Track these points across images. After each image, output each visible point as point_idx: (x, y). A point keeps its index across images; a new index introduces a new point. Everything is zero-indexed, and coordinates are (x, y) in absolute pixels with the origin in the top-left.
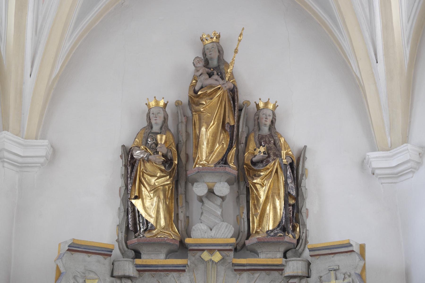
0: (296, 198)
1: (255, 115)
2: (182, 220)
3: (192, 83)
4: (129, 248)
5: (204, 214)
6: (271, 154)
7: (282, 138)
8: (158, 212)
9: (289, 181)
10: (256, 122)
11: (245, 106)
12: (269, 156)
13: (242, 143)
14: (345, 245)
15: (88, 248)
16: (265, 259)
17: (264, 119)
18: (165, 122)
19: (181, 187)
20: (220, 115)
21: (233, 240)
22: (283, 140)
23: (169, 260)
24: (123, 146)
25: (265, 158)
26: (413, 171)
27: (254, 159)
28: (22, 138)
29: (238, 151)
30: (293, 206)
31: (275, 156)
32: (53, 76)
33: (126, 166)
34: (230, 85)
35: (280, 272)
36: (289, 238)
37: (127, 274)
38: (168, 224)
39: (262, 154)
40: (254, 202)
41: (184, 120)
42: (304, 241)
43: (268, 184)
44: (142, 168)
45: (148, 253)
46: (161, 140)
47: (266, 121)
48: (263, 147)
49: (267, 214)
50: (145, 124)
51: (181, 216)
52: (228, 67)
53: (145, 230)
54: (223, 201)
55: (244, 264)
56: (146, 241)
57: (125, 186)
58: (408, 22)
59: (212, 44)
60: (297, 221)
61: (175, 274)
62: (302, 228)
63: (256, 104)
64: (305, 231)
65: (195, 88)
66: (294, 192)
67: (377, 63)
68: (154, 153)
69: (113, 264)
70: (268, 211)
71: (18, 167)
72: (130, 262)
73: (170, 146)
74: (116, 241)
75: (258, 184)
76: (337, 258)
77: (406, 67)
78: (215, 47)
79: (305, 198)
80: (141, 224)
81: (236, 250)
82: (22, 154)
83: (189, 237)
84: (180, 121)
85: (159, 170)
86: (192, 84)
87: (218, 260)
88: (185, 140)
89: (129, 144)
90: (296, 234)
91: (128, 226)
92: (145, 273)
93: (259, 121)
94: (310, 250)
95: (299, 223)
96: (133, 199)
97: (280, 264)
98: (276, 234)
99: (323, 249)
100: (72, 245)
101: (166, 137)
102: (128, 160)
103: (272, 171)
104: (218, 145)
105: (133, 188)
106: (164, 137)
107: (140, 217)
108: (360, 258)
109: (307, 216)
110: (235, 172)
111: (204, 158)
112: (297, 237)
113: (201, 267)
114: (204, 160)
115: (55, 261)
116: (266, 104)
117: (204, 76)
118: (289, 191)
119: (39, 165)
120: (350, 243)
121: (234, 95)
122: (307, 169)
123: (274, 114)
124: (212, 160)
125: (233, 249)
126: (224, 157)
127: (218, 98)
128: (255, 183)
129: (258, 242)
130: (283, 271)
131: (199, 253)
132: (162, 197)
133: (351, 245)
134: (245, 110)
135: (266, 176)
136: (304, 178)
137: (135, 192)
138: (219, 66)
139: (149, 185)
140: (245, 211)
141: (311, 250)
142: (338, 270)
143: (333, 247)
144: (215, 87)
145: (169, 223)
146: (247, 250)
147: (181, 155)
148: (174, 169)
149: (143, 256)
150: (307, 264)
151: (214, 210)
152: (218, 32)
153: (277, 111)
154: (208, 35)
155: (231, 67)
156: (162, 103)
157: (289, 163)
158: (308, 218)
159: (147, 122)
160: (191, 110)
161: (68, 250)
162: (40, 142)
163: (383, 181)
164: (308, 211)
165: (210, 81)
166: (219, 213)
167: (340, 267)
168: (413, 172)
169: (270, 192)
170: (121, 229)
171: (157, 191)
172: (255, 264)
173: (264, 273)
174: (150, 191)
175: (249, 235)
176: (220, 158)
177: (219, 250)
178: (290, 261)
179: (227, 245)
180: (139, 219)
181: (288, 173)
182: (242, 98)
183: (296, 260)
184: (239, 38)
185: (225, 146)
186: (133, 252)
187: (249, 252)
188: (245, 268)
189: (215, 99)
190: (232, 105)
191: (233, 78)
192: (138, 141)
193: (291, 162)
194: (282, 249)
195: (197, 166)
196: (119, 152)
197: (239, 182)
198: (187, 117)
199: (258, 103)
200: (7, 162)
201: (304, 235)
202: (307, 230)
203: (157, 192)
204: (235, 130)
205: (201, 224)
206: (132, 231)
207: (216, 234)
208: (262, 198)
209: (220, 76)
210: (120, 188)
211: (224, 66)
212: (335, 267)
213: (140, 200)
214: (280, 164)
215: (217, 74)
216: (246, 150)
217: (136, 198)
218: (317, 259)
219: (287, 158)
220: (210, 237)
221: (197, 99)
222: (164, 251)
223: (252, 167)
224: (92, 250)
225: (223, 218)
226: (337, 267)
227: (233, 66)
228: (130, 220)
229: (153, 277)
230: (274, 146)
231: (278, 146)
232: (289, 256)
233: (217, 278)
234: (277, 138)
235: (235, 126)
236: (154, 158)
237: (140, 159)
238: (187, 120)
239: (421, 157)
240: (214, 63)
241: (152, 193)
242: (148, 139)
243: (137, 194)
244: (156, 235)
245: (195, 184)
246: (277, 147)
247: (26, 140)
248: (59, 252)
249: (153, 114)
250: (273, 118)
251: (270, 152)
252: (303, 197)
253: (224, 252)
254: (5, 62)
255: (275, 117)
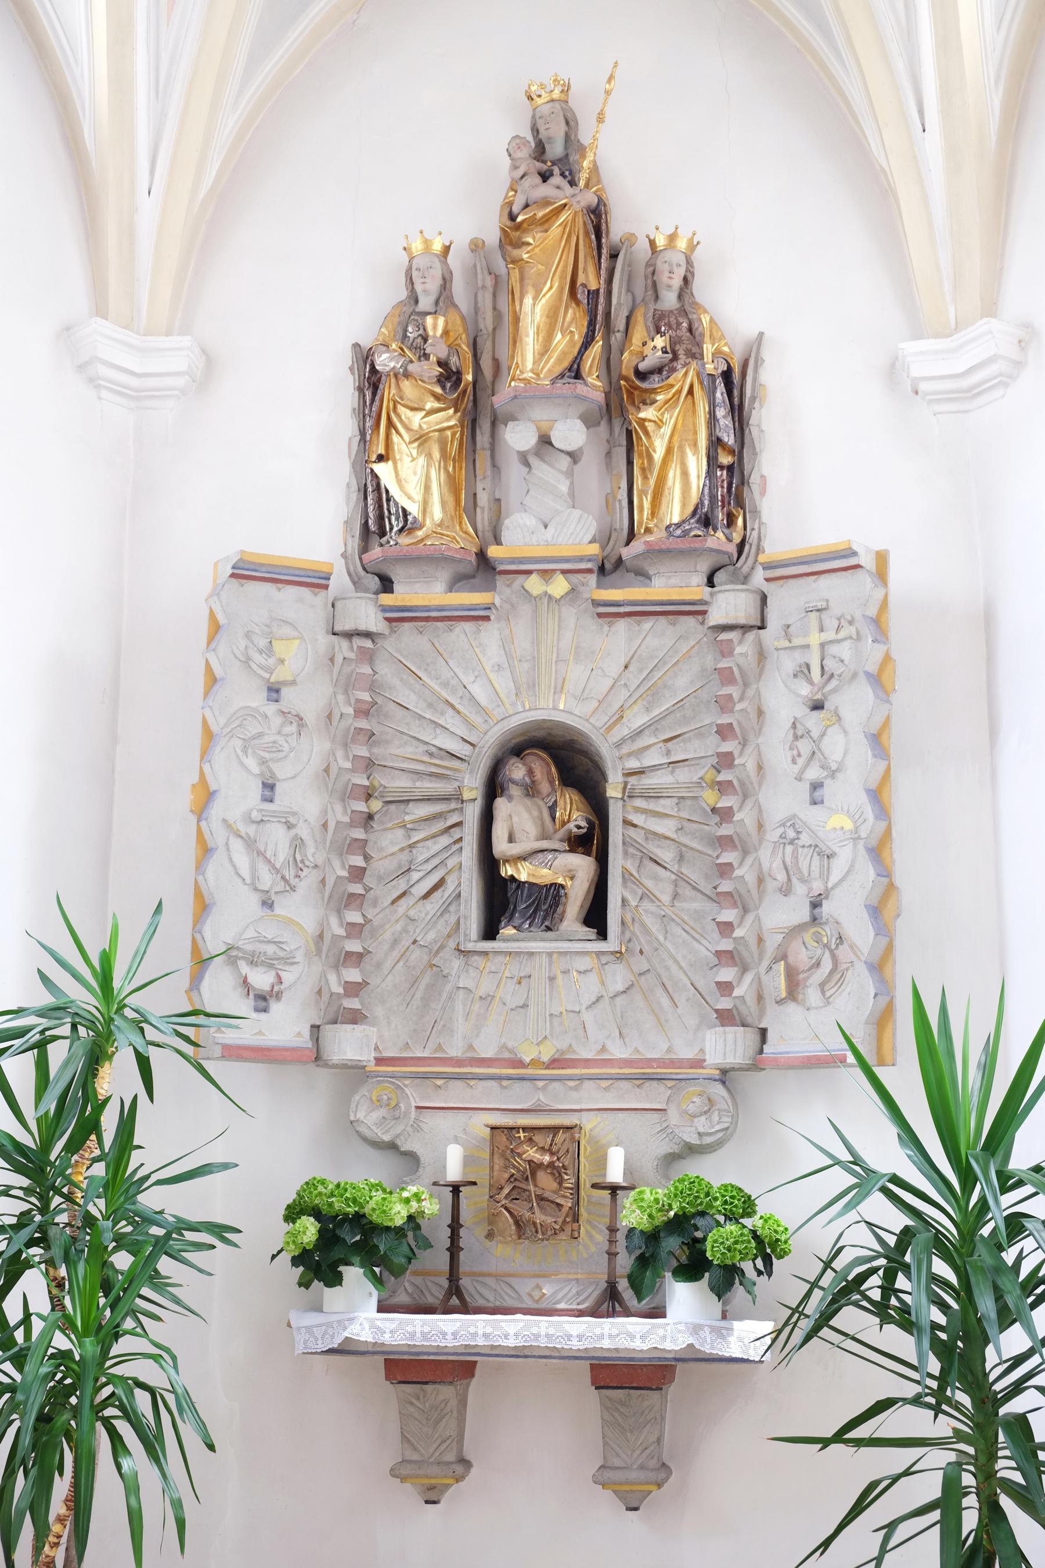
0: (739, 452)
1: (647, 265)
2: (484, 508)
3: (506, 197)
4: (368, 570)
5: (530, 492)
6: (681, 353)
7: (706, 315)
8: (427, 488)
9: (720, 413)
10: (649, 282)
11: (625, 247)
12: (675, 358)
13: (619, 331)
14: (842, 554)
15: (277, 570)
16: (664, 589)
17: (667, 274)
18: (445, 288)
19: (482, 434)
20: (566, 266)
21: (594, 549)
22: (708, 320)
23: (453, 595)
24: (356, 346)
25: (666, 361)
26: (1005, 381)
27: (643, 366)
28: (138, 333)
29: (607, 348)
30: (730, 468)
31: (688, 358)
32: (202, 193)
33: (360, 390)
34: (589, 198)
35: (700, 618)
36: (717, 539)
37: (362, 627)
38: (451, 516)
39: (660, 352)
40: (643, 463)
41: (489, 282)
42: (754, 548)
43: (670, 419)
44: (393, 391)
45: (408, 580)
46: (435, 327)
47: (671, 278)
48: (661, 336)
49: (669, 489)
50: (403, 294)
51: (483, 499)
52: (583, 157)
53: (401, 531)
54: (575, 462)
55: (619, 601)
56: (401, 554)
57: (358, 433)
58: (999, 28)
59: (550, 105)
60: (740, 504)
61: (468, 626)
62: (750, 518)
63: (650, 241)
64: (756, 526)
65: (511, 209)
66: (732, 436)
67: (924, 131)
68: (420, 357)
69: (333, 606)
70: (670, 482)
71: (132, 398)
72: (369, 602)
73: (456, 342)
74: (342, 555)
75: (650, 421)
76: (824, 581)
77: (994, 138)
78: (556, 111)
79: (758, 450)
80: (393, 518)
81: (602, 570)
82: (137, 370)
83: (498, 542)
84: (480, 284)
85: (430, 395)
86: (507, 201)
87: (562, 593)
88: (490, 328)
89: (366, 343)
90: (735, 531)
91: (366, 522)
92: (403, 624)
93: (655, 278)
94: (765, 566)
95: (743, 508)
96: (375, 462)
97: (699, 600)
98: (686, 533)
99: (794, 564)
100: (241, 565)
101: (446, 322)
102: (365, 375)
103: (679, 391)
104: (559, 336)
105: (374, 438)
106: (441, 321)
107: (391, 503)
108: (874, 582)
109: (763, 492)
110: (599, 397)
111: (529, 365)
112: (737, 538)
113: (525, 609)
114: (528, 369)
115: (206, 600)
116: (672, 238)
117: (529, 180)
118: (720, 435)
119: (177, 392)
120: (851, 548)
121: (600, 221)
122: (764, 386)
123: (689, 262)
124: (546, 370)
125: (596, 569)
126: (574, 362)
127: (561, 229)
128: (644, 420)
129: (648, 551)
130: (706, 616)
131: (521, 578)
132: (436, 455)
133: (855, 554)
134: (625, 254)
135: (667, 402)
136: (757, 405)
137: (378, 445)
138: (567, 155)
139: (408, 429)
140: (624, 485)
141: (767, 567)
142: (825, 609)
143: (814, 558)
144: (555, 203)
145: (453, 514)
146: (627, 571)
147: (481, 362)
148: (465, 391)
149: (396, 587)
150: (758, 598)
151: (555, 483)
152: (564, 76)
153: (697, 256)
154: (542, 86)
155: (590, 156)
156: (437, 246)
157: (720, 371)
158: (764, 495)
159: (407, 289)
160: (505, 259)
161: (233, 575)
162: (175, 341)
163: (938, 408)
164: (765, 481)
165: (545, 190)
166: (564, 487)
167: (831, 604)
168: (1006, 385)
169: (676, 437)
170: (351, 529)
171: (425, 441)
172: (643, 601)
173: (662, 620)
174: (411, 442)
175: (631, 536)
176: (566, 364)
177: (564, 572)
178: (719, 592)
179: (581, 559)
180: (388, 505)
181: (718, 395)
182: (617, 229)
183: (734, 590)
184: (607, 86)
185: (576, 337)
186: (376, 578)
187: (633, 575)
188: (622, 610)
189: (555, 229)
190: (594, 244)
191: (599, 182)
192: (386, 332)
193: (725, 369)
194: (704, 566)
195: (513, 384)
196: (347, 358)
197: (610, 420)
198: (496, 277)
199: (652, 238)
200: (107, 388)
201: (755, 534)
202: (761, 524)
203: (427, 445)
204: (602, 300)
205: (524, 515)
206: (374, 532)
207: (555, 536)
208: (658, 455)
209: (569, 178)
210: (350, 439)
211: (578, 157)
212: (820, 604)
213: (390, 462)
214: (698, 375)
215: (562, 175)
216: (627, 345)
217: (381, 458)
218: (782, 586)
219: (715, 361)
220: (542, 543)
221: (518, 233)
222: (444, 576)
223: (638, 383)
224: (285, 574)
225: (573, 499)
226: (825, 604)
227: (595, 154)
228: (371, 508)
229: (421, 633)
230: (688, 334)
231: (697, 334)
232: (719, 581)
233: (559, 632)
234: (695, 316)
235: (602, 291)
236: (419, 369)
237: (390, 371)
238: (496, 282)
239: (1022, 349)
240: (556, 150)
241: (414, 448)
242: (407, 326)
243: (381, 450)
244: (422, 540)
245: (510, 424)
246: (695, 337)
247: (143, 338)
248: (214, 581)
249: (418, 269)
250: (686, 271)
251: (677, 347)
252: (754, 448)
253: (576, 575)
254: (94, 165)
255: (691, 269)
